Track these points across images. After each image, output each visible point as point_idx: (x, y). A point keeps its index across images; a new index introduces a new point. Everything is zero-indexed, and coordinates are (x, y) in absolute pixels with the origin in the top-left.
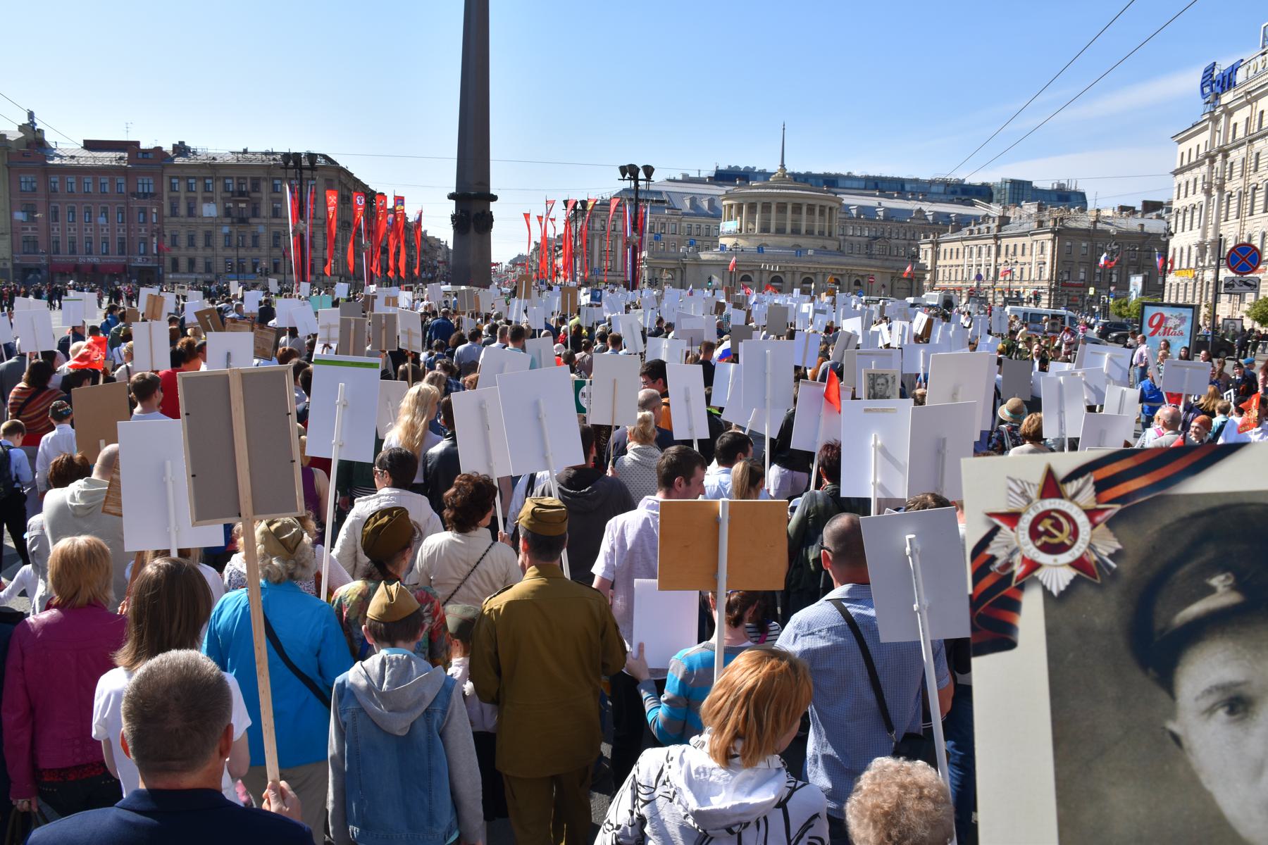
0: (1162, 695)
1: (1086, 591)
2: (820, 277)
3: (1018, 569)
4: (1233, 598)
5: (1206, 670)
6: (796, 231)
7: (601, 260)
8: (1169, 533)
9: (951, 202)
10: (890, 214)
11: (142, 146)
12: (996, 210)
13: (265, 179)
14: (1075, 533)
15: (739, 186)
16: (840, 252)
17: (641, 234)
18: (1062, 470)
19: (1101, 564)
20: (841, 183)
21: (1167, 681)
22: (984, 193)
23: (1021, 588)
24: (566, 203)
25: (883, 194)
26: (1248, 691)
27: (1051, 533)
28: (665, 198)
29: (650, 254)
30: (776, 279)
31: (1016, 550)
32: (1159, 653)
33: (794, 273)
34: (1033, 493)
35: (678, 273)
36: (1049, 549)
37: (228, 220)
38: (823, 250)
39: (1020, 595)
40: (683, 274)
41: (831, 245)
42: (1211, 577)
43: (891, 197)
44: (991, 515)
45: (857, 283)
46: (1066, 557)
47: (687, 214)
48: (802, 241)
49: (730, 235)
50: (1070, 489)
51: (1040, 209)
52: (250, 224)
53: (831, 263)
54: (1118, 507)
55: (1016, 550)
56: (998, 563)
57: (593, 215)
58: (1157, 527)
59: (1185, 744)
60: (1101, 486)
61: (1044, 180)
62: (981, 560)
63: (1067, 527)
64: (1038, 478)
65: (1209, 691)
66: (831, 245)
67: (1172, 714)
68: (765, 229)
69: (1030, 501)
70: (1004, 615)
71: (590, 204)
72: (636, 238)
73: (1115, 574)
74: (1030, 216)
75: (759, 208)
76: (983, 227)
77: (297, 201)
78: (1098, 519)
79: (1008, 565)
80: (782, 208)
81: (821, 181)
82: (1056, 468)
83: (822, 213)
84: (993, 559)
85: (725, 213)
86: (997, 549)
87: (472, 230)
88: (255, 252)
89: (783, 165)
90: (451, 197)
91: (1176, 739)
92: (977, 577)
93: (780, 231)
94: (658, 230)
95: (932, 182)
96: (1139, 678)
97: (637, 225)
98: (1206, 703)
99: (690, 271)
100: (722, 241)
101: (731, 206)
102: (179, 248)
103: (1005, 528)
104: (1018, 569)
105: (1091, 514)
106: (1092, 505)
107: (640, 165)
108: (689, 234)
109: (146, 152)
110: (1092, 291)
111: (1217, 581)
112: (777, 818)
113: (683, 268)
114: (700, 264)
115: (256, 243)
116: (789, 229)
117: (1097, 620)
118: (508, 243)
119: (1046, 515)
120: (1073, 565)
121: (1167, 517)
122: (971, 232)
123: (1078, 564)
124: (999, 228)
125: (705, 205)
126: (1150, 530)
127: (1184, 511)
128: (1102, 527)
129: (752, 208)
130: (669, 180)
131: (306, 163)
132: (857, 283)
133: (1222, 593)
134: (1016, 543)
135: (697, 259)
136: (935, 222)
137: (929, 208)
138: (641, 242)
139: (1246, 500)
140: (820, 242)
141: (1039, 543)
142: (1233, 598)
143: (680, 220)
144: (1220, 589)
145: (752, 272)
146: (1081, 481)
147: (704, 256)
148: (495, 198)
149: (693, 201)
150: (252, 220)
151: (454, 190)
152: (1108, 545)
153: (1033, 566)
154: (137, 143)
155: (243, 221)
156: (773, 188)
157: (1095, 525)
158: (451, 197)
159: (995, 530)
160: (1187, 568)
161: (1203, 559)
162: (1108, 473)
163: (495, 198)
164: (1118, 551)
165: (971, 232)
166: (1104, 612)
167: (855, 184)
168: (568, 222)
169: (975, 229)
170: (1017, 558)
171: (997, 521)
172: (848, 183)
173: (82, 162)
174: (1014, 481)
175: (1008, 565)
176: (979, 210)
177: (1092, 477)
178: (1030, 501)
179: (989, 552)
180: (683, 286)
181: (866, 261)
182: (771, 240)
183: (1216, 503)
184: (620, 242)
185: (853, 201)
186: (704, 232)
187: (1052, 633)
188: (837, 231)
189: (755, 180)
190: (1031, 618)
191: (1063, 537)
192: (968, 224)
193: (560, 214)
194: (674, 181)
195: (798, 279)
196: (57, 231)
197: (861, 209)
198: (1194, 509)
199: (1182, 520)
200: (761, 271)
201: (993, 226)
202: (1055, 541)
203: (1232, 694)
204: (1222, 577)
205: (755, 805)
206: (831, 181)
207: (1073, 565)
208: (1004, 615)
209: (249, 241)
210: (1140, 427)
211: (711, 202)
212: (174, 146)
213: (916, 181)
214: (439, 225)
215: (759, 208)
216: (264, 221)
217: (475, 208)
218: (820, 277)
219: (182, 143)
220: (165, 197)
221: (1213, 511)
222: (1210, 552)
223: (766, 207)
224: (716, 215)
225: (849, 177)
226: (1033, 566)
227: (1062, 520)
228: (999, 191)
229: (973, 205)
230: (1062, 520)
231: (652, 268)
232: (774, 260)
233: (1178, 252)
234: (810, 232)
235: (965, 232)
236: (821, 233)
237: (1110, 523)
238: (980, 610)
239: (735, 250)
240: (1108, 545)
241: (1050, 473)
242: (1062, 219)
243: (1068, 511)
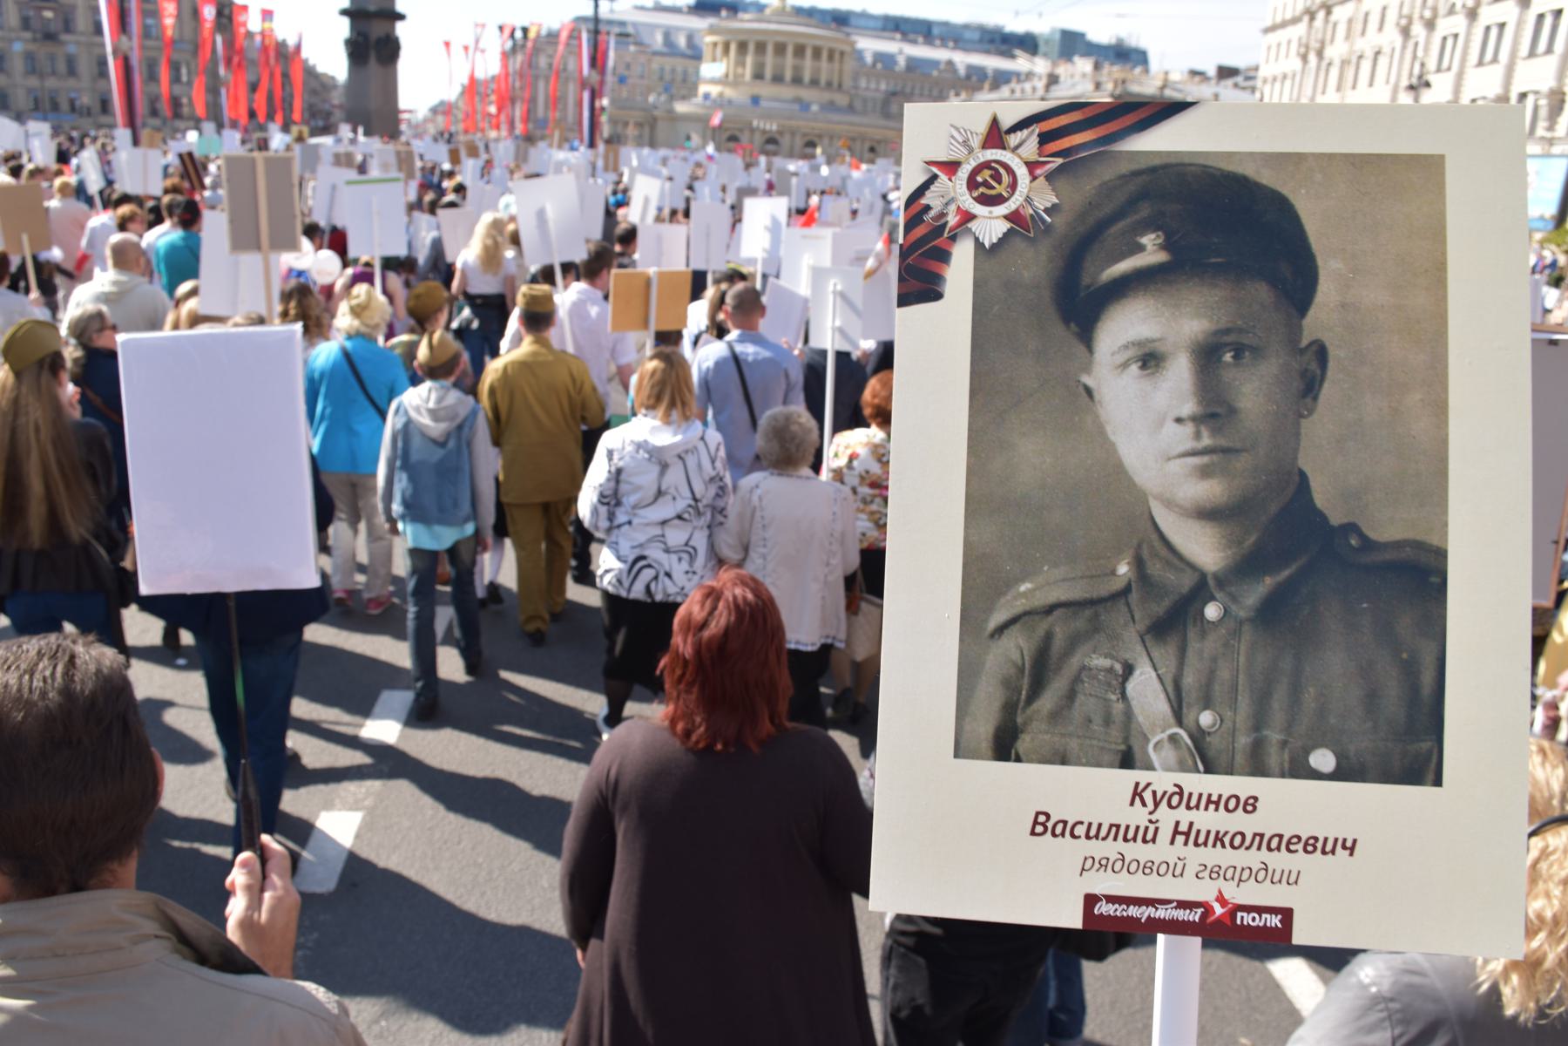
0: (1080, 349)
1: (1019, 244)
2: (826, 141)
3: (952, 220)
4: (1161, 257)
5: (1126, 325)
6: (797, 80)
7: (546, 107)
8: (1107, 190)
9: (988, 52)
10: (914, 64)
12: (1041, 66)
14: (1013, 186)
15: (727, 18)
16: (851, 109)
17: (603, 72)
18: (1007, 121)
19: (1036, 218)
20: (853, 21)
21: (1086, 337)
22: (1028, 44)
23: (953, 238)
24: (501, 28)
26: (1160, 348)
27: (988, 185)
28: (630, 30)
29: (612, 102)
30: (771, 140)
31: (952, 200)
32: (1080, 307)
33: (793, 134)
34: (976, 142)
35: (647, 131)
36: (986, 200)
37: (28, 35)
38: (830, 106)
39: (951, 246)
40: (653, 130)
41: (841, 100)
42: (1142, 235)
43: (914, 42)
44: (928, 163)
45: (872, 150)
46: (1002, 210)
47: (656, 53)
48: (806, 94)
49: (713, 81)
50: (1013, 140)
51: (1097, 67)
52: (62, 43)
53: (842, 123)
54: (1060, 161)
55: (952, 200)
56: (932, 213)
57: (537, 50)
58: (1096, 183)
59: (1097, 397)
60: (1045, 139)
61: (1101, 34)
62: (915, 209)
63: (1006, 178)
64: (982, 127)
65: (1126, 347)
66: (841, 100)
67: (1087, 368)
68: (758, 76)
69: (971, 151)
70: (933, 265)
71: (532, 35)
72: (595, 77)
73: (1048, 228)
74: (1084, 75)
75: (751, 47)
76: (1028, 86)
78: (1038, 172)
79: (942, 215)
80: (780, 49)
81: (828, 18)
82: (1000, 118)
83: (831, 57)
84: (928, 208)
85: (707, 52)
86: (931, 198)
88: (71, 83)
90: (344, 12)
91: (1089, 392)
92: (909, 227)
93: (778, 79)
94: (622, 71)
95: (966, 27)
96: (1060, 332)
97: (597, 60)
98: (1121, 358)
99: (662, 129)
100: (703, 89)
101: (715, 44)
103: (943, 177)
104: (952, 220)
105: (1031, 166)
106: (1034, 157)
108: (661, 78)
111: (1149, 240)
112: (701, 445)
113: (652, 123)
114: (673, 117)
115: (72, 71)
116: (788, 75)
117: (1026, 274)
118: (425, 81)
119: (986, 165)
120: (1007, 217)
121: (1107, 173)
122: (1013, 91)
123: (1013, 217)
124: (1048, 87)
125: (682, 41)
126: (1087, 186)
127: (1125, 168)
128: (1041, 180)
129: (742, 47)
132: (872, 150)
133: (1151, 251)
134: (954, 193)
135: (671, 111)
136: (968, 77)
137: (963, 60)
138: (602, 83)
139: (1187, 160)
140: (827, 96)
141: (976, 194)
142: (1161, 257)
143: (650, 61)
144: (1150, 247)
145: (741, 130)
146: (1026, 132)
147: (681, 108)
148: (401, 17)
149: (667, 35)
150: (64, 37)
152: (1045, 198)
153: (968, 217)
155: (50, 37)
156: (769, 22)
157: (1034, 178)
158: (344, 12)
159: (934, 177)
160: (1120, 225)
161: (1137, 217)
162: (1054, 125)
163: (401, 17)
164: (1054, 206)
165: (1013, 91)
166: (1034, 266)
167: (872, 24)
168: (505, 56)
169: (1018, 88)
170: (953, 208)
171: (935, 170)
172: (862, 22)
174: (957, 129)
175: (942, 215)
176: (1021, 63)
177: (1036, 129)
178: (971, 151)
179: (924, 201)
180: (653, 144)
181: (882, 122)
182: (766, 90)
183: (1157, 162)
184: (572, 88)
185: (869, 45)
186: (679, 78)
187: (978, 285)
188: (848, 83)
189: (745, 10)
190: (960, 271)
191: (1000, 189)
192: (1008, 81)
193: (494, 46)
194: (642, 8)
195: (799, 142)
197: (879, 57)
198: (1134, 167)
199: (1123, 177)
200: (752, 130)
201: (1040, 85)
202: (993, 192)
203: (1147, 350)
204: (1153, 236)
206: (840, 19)
207: (1007, 217)
208: (933, 265)
209: (62, 66)
211: (690, 38)
213: (946, 24)
214: (328, 54)
215: (751, 47)
216: (82, 39)
217: (377, 30)
218: (826, 141)
221: (1153, 170)
222: (1145, 211)
223: (761, 48)
224: (696, 55)
225: (864, 15)
226: (968, 217)
227: (1002, 171)
228: (1047, 42)
229: (1013, 57)
230: (1002, 171)
231: (613, 121)
232: (768, 116)
234: (814, 82)
235: (1005, 91)
236: (829, 84)
237: (1049, 177)
238: (909, 261)
239: (721, 102)
240: (1045, 198)
241: (995, 122)
242: (1124, 82)
243: (1015, 168)
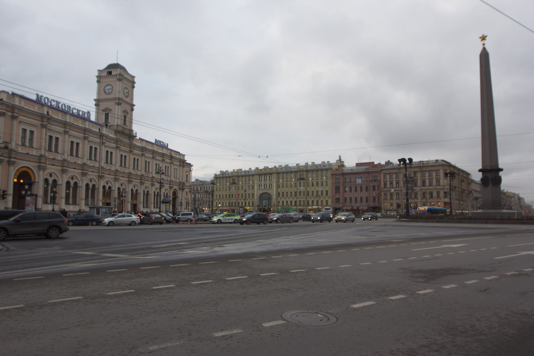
11: (375, 163)
13: (419, 172)
25: (69, 198)
77: (352, 172)
87: (490, 185)
88: (416, 200)
90: (480, 171)
109: (376, 165)
148: (501, 170)
151: (481, 167)
154: (373, 163)
158: (480, 171)
163: (501, 170)
173: (219, 253)
210: (115, 128)
212: (386, 163)
219: (389, 161)
220: (382, 181)
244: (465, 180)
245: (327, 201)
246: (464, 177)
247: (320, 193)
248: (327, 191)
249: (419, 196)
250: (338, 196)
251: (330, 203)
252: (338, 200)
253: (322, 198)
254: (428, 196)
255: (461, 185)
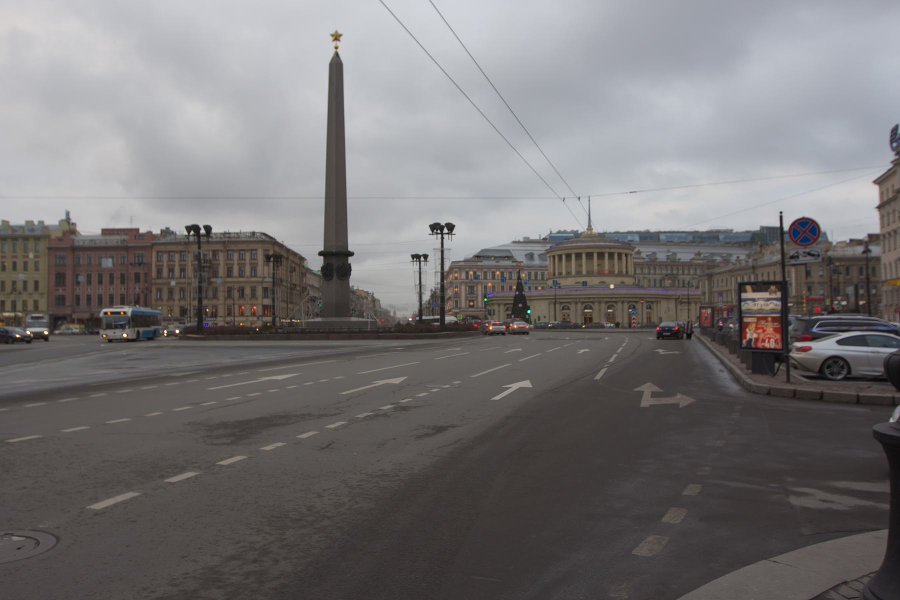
13: (222, 251)
87: (335, 278)
88: (215, 302)
89: (590, 226)
90: (321, 254)
102: (174, 300)
107: (443, 224)
109: (143, 235)
110: (520, 305)
130: (514, 242)
131: (203, 231)
140: (619, 279)
148: (352, 254)
154: (137, 230)
156: (582, 242)
158: (321, 254)
163: (352, 254)
194: (519, 242)
196: (78, 291)
205: (845, 395)
219: (168, 229)
233: (888, 266)
244: (297, 268)
245: (36, 303)
246: (296, 264)
247: (20, 286)
248: (36, 283)
249: (221, 295)
250: (61, 292)
251: (43, 305)
252: (61, 300)
253: (25, 296)
254: (236, 294)
255: (291, 277)
